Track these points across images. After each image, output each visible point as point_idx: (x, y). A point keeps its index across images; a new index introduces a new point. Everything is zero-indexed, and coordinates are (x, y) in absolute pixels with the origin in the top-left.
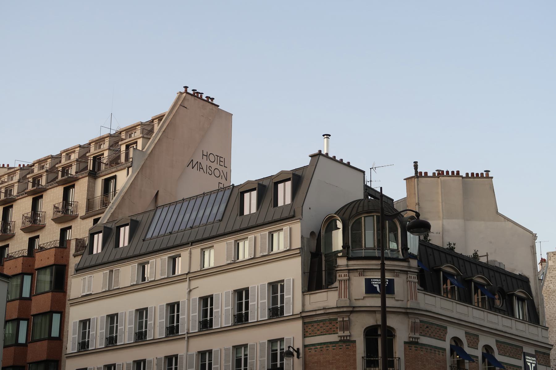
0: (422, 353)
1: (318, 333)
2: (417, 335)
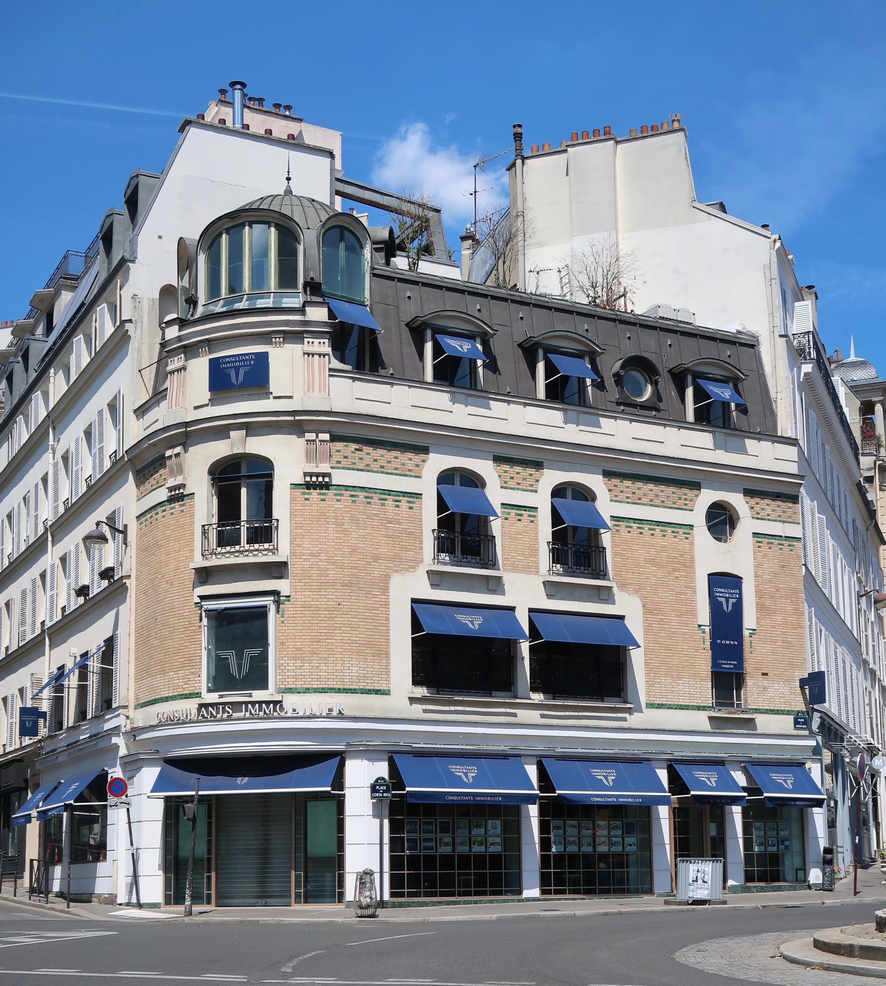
0: (338, 505)
1: (774, 516)
2: (324, 468)
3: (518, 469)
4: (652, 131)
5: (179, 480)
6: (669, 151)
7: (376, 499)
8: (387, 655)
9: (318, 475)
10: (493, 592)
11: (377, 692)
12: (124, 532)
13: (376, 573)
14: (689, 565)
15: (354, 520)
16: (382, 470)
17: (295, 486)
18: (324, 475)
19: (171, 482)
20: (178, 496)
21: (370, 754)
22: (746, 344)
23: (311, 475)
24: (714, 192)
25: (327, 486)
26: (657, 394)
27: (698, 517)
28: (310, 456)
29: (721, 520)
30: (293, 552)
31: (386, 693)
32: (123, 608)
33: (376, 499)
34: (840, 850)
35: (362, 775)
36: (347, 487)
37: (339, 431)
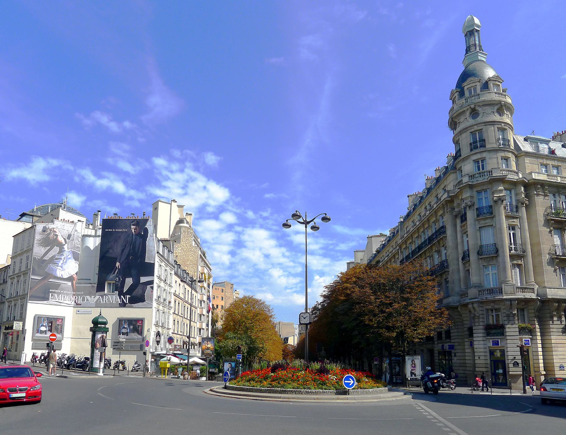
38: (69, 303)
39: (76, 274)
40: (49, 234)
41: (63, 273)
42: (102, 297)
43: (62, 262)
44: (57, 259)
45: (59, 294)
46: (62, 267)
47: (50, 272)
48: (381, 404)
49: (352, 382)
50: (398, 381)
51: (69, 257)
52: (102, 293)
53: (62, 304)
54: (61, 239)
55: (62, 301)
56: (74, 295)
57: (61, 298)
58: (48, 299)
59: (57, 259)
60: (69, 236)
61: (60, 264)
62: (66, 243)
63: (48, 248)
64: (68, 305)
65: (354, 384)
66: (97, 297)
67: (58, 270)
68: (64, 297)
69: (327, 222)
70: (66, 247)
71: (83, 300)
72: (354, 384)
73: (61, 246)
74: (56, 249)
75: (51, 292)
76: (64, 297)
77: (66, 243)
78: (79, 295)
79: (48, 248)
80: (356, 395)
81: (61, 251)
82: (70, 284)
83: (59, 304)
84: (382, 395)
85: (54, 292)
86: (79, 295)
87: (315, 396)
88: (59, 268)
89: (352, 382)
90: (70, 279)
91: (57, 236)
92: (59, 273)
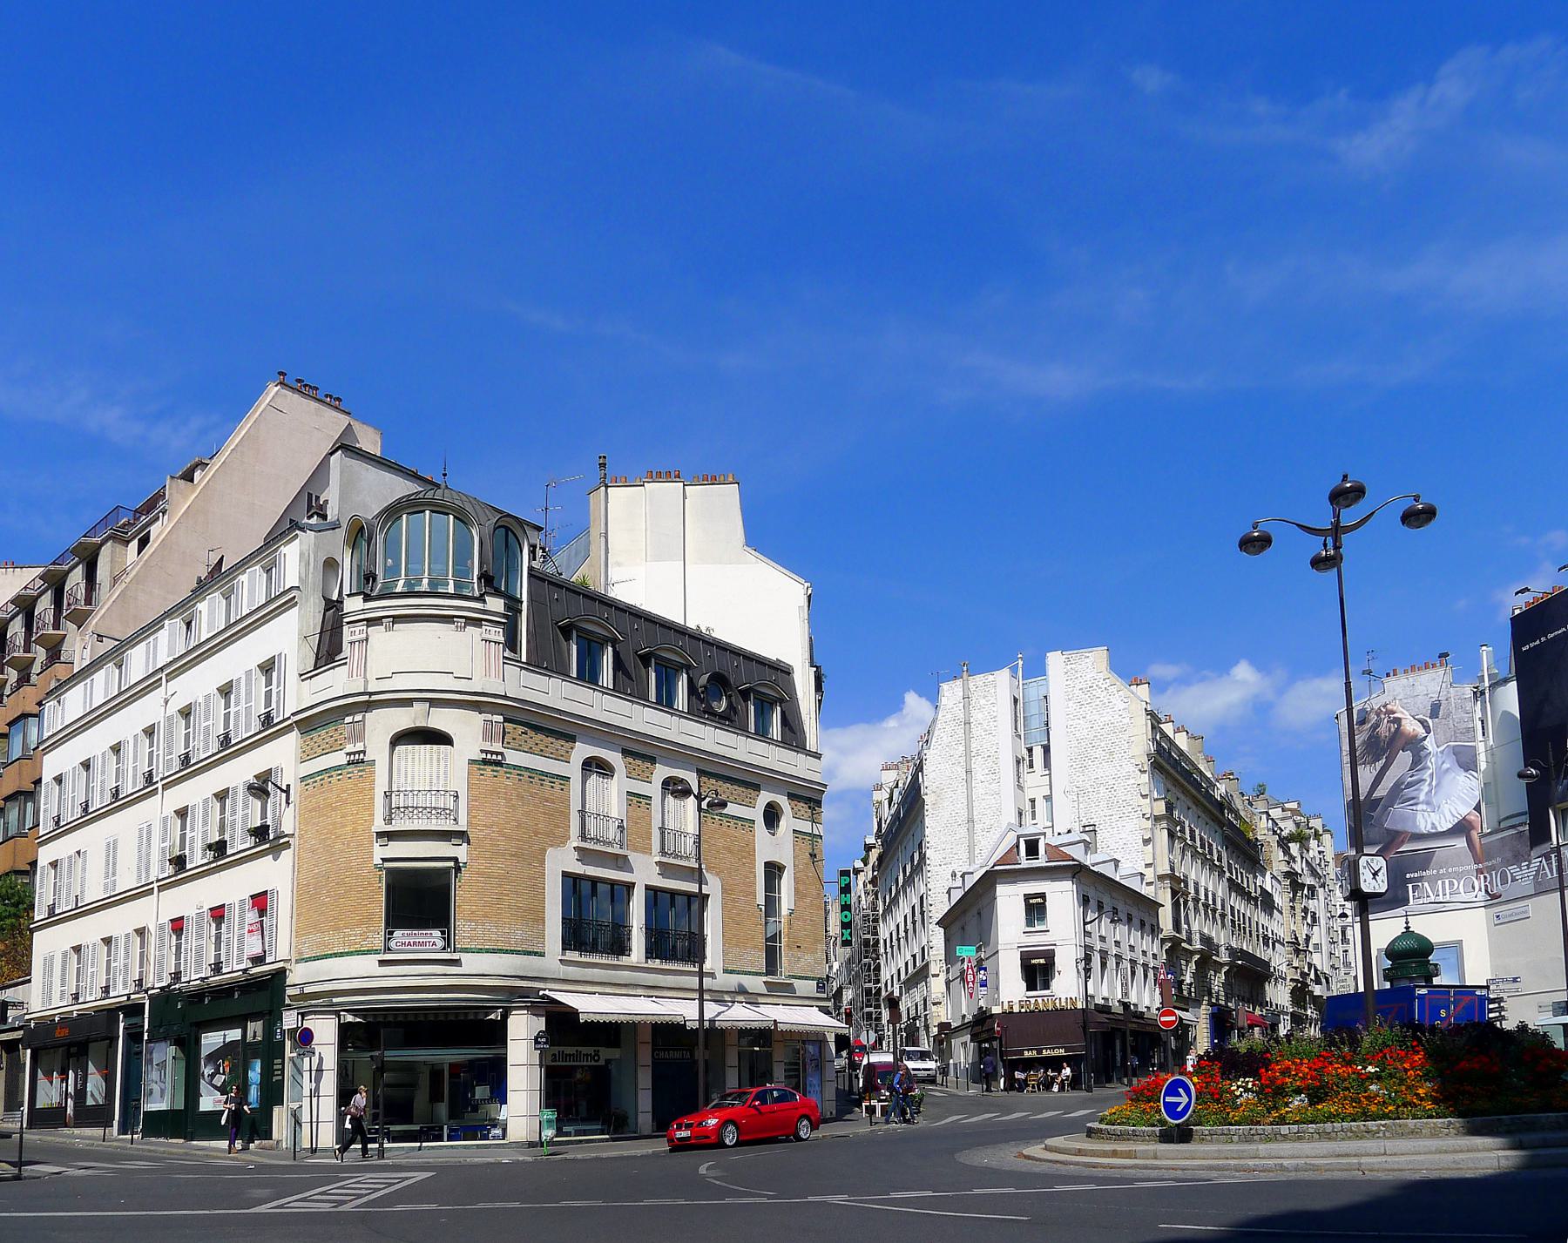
0: (508, 782)
2: (497, 747)
3: (639, 762)
4: (713, 481)
5: (360, 746)
6: (728, 496)
7: (536, 780)
8: (543, 919)
9: (492, 753)
10: (620, 869)
11: (536, 954)
12: (287, 791)
13: (536, 847)
14: (751, 854)
15: (520, 797)
16: (541, 754)
17: (472, 762)
18: (497, 754)
19: (350, 748)
20: (358, 761)
21: (534, 1009)
22: (782, 671)
23: (487, 752)
24: (767, 535)
25: (498, 764)
26: (730, 706)
27: (757, 814)
28: (488, 735)
29: (772, 816)
30: (469, 823)
31: (542, 955)
32: (1088, 863)
33: (536, 780)
34: (238, 1144)
35: (522, 1029)
36: (515, 767)
37: (510, 715)
38: (1470, 897)
39: (1478, 808)
40: (1376, 726)
41: (1434, 817)
42: (1548, 858)
43: (1425, 788)
44: (1410, 785)
45: (1433, 881)
46: (1428, 803)
47: (1399, 827)
48: (1337, 1175)
49: (1184, 1100)
50: (209, 1101)
51: (1446, 766)
52: (1545, 848)
53: (1451, 906)
54: (1411, 727)
55: (1447, 898)
56: (1479, 871)
57: (1443, 890)
58: (1405, 902)
59: (1410, 785)
60: (1435, 710)
61: (1422, 797)
62: (1428, 732)
63: (1379, 764)
64: (1468, 906)
65: (1188, 1104)
66: (1536, 862)
67: (1419, 816)
68: (1451, 884)
69: (1263, 548)
70: (1430, 744)
71: (1504, 881)
72: (1188, 1104)
73: (1415, 745)
74: (1405, 758)
75: (1411, 880)
76: (1451, 884)
77: (1428, 732)
78: (1493, 868)
79: (1379, 764)
80: (1218, 1142)
81: (1417, 762)
82: (1461, 843)
83: (1439, 907)
84: (1140, 1147)
85: (1420, 879)
86: (1493, 868)
87: (1108, 1147)
88: (1420, 807)
89: (1184, 1100)
90: (1462, 828)
91: (1398, 721)
92: (1424, 823)
